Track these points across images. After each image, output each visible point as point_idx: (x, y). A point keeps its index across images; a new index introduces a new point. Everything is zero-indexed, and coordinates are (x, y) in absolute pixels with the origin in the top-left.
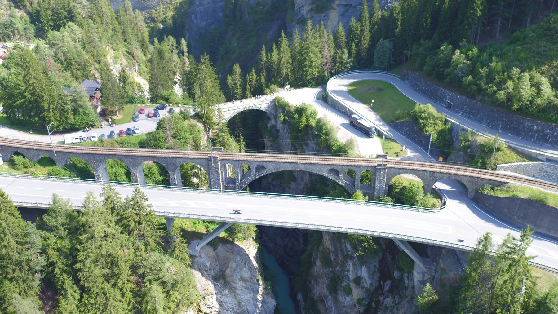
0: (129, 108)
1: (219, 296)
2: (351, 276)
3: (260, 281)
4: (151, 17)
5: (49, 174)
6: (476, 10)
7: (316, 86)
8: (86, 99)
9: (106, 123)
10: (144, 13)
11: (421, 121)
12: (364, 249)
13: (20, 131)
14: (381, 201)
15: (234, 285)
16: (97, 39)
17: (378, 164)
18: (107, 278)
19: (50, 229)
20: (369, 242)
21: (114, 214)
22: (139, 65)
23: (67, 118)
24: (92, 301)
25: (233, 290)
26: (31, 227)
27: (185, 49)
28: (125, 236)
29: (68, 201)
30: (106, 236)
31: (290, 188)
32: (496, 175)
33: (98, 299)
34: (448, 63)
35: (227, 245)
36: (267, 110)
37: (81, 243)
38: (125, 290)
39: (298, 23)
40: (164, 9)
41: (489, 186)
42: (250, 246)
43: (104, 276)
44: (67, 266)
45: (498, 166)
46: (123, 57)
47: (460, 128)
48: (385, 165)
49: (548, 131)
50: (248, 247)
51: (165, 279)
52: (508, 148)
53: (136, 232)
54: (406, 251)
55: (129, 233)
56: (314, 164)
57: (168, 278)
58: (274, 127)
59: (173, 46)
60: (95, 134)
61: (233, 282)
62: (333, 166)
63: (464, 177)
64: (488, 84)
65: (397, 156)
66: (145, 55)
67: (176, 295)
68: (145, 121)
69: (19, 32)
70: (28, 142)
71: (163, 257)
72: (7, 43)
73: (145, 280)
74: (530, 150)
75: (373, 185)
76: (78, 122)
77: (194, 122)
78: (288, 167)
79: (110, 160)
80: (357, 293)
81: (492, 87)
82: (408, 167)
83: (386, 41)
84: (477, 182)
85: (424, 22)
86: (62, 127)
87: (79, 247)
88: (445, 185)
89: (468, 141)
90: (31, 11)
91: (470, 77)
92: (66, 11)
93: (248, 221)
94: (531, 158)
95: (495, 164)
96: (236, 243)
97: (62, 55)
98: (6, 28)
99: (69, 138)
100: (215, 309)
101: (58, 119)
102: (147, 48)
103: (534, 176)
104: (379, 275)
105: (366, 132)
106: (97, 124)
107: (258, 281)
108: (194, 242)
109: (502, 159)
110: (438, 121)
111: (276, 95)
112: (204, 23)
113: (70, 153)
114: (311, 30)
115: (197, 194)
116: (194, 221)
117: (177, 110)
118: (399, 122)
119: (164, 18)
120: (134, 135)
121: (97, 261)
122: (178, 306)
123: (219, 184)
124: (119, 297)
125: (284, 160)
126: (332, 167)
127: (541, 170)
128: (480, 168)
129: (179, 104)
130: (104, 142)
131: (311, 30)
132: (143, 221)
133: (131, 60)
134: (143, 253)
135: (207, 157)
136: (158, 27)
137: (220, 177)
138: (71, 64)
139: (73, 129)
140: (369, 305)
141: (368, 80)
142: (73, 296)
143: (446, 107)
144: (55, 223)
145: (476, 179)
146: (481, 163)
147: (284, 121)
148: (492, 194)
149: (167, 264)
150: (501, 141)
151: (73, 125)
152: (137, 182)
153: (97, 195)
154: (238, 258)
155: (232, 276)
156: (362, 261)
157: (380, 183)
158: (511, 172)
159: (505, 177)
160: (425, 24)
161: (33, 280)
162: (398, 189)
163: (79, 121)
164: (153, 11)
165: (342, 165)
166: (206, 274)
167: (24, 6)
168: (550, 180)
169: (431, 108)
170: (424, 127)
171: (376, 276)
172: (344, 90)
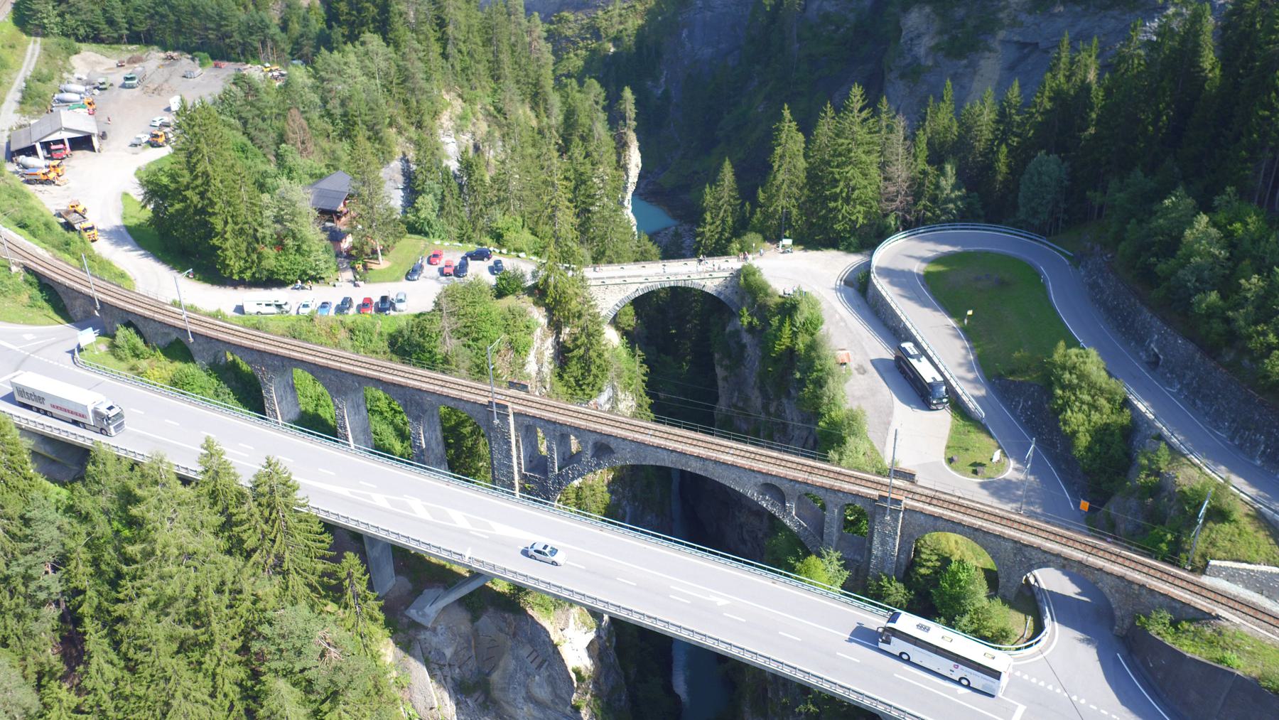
7: (849, 249)
10: (580, 15)
11: (1059, 392)
17: (880, 496)
21: (216, 508)
23: (261, 257)
32: (1197, 589)
34: (1172, 244)
35: (506, 615)
36: (720, 293)
38: (221, 681)
40: (623, 11)
41: (1167, 616)
45: (1212, 562)
46: (480, 116)
47: (1154, 433)
48: (898, 502)
50: (562, 627)
57: (321, 675)
59: (597, 103)
61: (508, 703)
62: (770, 478)
63: (1104, 576)
64: (1256, 323)
65: (975, 472)
66: (537, 116)
70: (152, 302)
75: (867, 545)
76: (282, 266)
78: (664, 460)
81: (1264, 334)
83: (1053, 157)
84: (1138, 596)
85: (1149, 124)
88: (1065, 580)
89: (1158, 473)
91: (1213, 296)
95: (1203, 556)
96: (530, 612)
97: (338, 106)
98: (251, 34)
99: (254, 299)
101: (244, 255)
102: (545, 101)
108: (429, 593)
109: (1228, 545)
110: (1102, 402)
111: (754, 261)
114: (861, 110)
115: (444, 486)
118: (1014, 382)
119: (621, 32)
120: (392, 313)
125: (657, 441)
128: (1164, 560)
129: (522, 251)
131: (861, 110)
136: (605, 50)
139: (271, 281)
141: (987, 253)
143: (1147, 363)
145: (1136, 587)
146: (1169, 543)
148: (1169, 640)
151: (272, 272)
154: (525, 652)
157: (883, 543)
158: (1247, 587)
159: (1219, 598)
160: (1151, 128)
162: (928, 567)
164: (600, 13)
165: (791, 480)
166: (439, 673)
169: (1093, 363)
170: (1063, 409)
172: (915, 271)
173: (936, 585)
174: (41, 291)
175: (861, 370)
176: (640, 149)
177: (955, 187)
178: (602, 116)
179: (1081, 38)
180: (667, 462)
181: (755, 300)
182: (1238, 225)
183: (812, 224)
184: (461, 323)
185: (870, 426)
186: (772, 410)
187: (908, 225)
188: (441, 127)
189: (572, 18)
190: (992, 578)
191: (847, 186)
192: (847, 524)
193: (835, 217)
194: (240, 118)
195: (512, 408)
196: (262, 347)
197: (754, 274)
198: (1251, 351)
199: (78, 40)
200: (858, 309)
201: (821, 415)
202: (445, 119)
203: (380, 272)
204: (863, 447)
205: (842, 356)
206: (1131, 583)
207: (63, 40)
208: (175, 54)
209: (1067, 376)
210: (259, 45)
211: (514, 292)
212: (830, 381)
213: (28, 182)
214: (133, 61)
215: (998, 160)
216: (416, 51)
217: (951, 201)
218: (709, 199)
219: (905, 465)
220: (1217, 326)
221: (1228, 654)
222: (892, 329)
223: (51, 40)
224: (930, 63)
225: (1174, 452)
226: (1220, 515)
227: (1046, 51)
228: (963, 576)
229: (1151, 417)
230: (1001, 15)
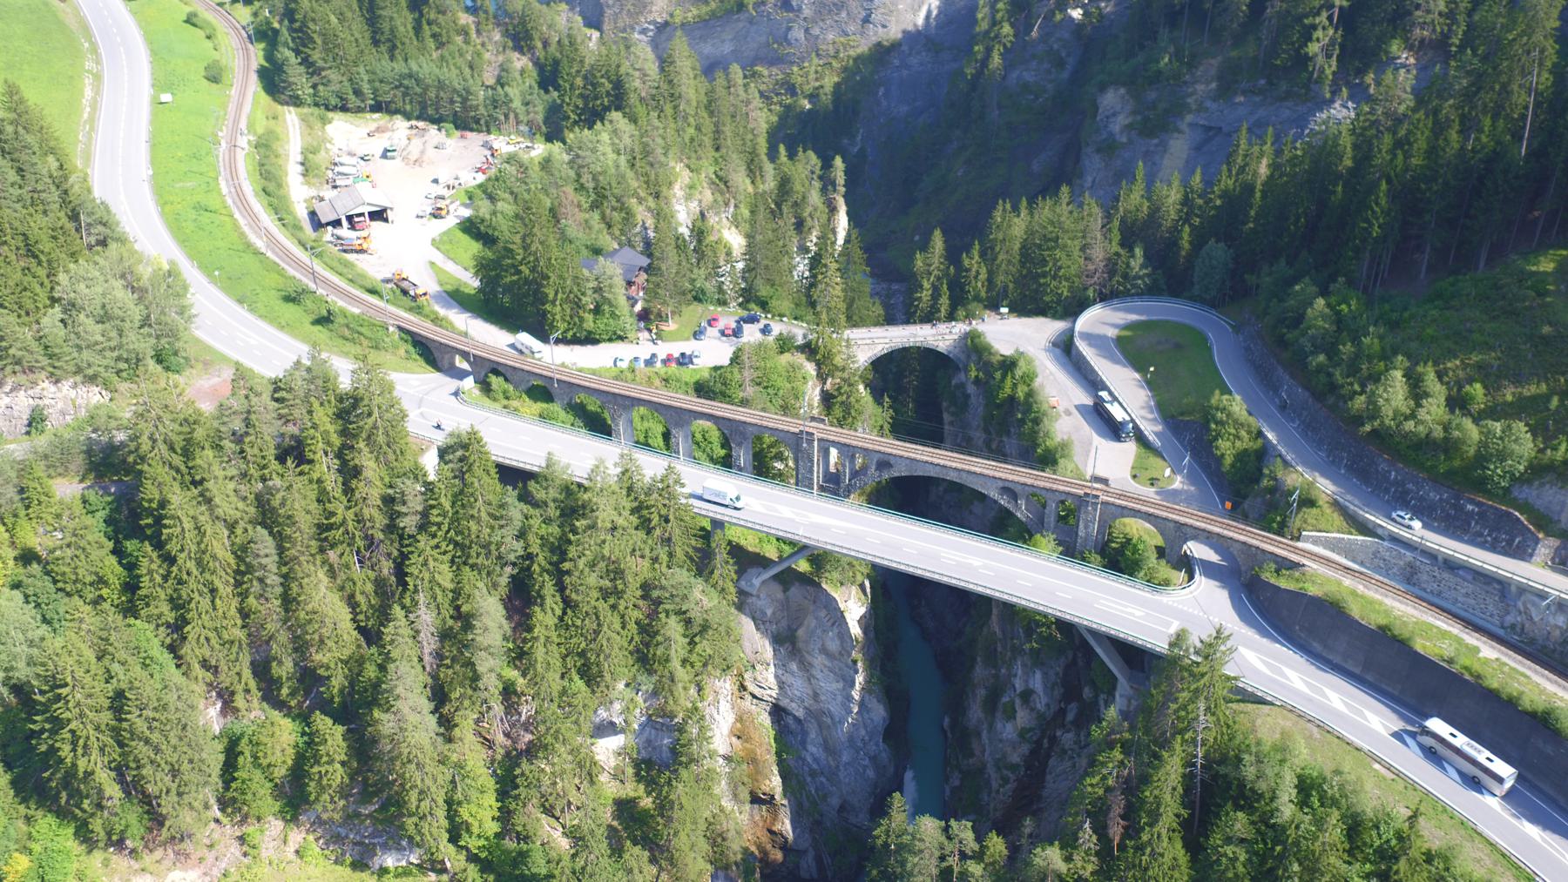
0: (695, 312)
1: (780, 672)
2: (1019, 685)
3: (860, 664)
4: (787, 83)
5: (540, 416)
6: (1371, 224)
7: (1056, 316)
8: (619, 282)
9: (646, 334)
10: (775, 70)
11: (1213, 426)
12: (1043, 639)
13: (501, 328)
14: (1083, 559)
15: (809, 658)
16: (659, 151)
18: (605, 594)
19: (536, 504)
20: (1049, 627)
22: (736, 206)
23: (582, 320)
24: (579, 623)
25: (806, 667)
26: (511, 495)
27: (840, 177)
28: (641, 534)
29: (568, 466)
30: (614, 529)
31: (971, 512)
33: (587, 622)
34: (1298, 319)
37: (575, 532)
39: (1098, 151)
41: (1273, 566)
42: (849, 598)
43: (601, 589)
44: (550, 564)
48: (1097, 497)
49: (1410, 486)
51: (691, 614)
52: (1332, 504)
53: (658, 532)
54: (1099, 650)
55: (649, 532)
56: (975, 473)
57: (695, 614)
58: (962, 386)
59: (813, 172)
60: (622, 353)
66: (753, 182)
67: (704, 647)
68: (717, 342)
69: (516, 116)
71: (692, 580)
72: (493, 136)
73: (660, 610)
74: (1367, 516)
77: (800, 359)
79: (642, 408)
80: (1023, 717)
81: (1351, 384)
82: (1138, 507)
83: (1221, 245)
86: (571, 333)
87: (572, 538)
89: (1275, 479)
90: (543, 60)
91: (1322, 358)
92: (610, 82)
93: (853, 553)
94: (1364, 528)
96: (824, 586)
98: (496, 107)
100: (769, 692)
101: (568, 318)
102: (761, 168)
103: (1362, 564)
104: (1062, 690)
105: (1114, 430)
106: (631, 335)
107: (855, 662)
108: (752, 571)
110: (1243, 433)
111: (976, 325)
112: (904, 109)
113: (579, 386)
116: (761, 535)
117: (777, 328)
119: (817, 88)
121: (594, 565)
122: (705, 665)
123: (812, 479)
124: (617, 626)
125: (925, 458)
126: (1007, 484)
127: (1376, 554)
130: (637, 373)
132: (671, 517)
133: (722, 193)
134: (664, 569)
135: (797, 430)
137: (815, 469)
138: (605, 197)
139: (590, 340)
140: (1039, 743)
141: (1167, 321)
142: (552, 609)
144: (544, 496)
147: (977, 381)
148: (1272, 581)
149: (697, 594)
150: (1325, 487)
151: (590, 332)
152: (678, 453)
153: (610, 464)
155: (807, 642)
156: (1037, 660)
157: (1086, 527)
161: (501, 575)
163: (602, 327)
164: (795, 69)
167: (531, 48)
168: (1387, 576)
169: (1237, 405)
170: (1216, 439)
171: (1056, 692)
173: (1123, 554)
174: (414, 347)
175: (1068, 413)
176: (848, 213)
177: (1143, 266)
178: (817, 184)
179: (1257, 131)
180: (932, 473)
181: (980, 358)
182: (1344, 307)
183: (1025, 296)
184: (755, 375)
185: (1077, 451)
186: (994, 446)
187: (1103, 298)
188: (674, 196)
189: (766, 73)
190: (1161, 552)
191: (1054, 265)
192: (1061, 519)
193: (1045, 290)
194: (512, 193)
195: (817, 435)
196: (616, 391)
197: (979, 337)
198: (1343, 396)
199: (327, 108)
200: (1063, 366)
201: (1039, 445)
202: (678, 191)
203: (670, 332)
204: (1070, 466)
205: (1053, 401)
206: (1251, 546)
207: (316, 111)
208: (421, 124)
209: (1219, 414)
210: (502, 118)
211: (789, 350)
212: (1045, 419)
213: (345, 251)
214: (379, 130)
215: (1182, 238)
216: (657, 128)
217: (1140, 278)
218: (919, 263)
219: (1101, 473)
220: (1322, 378)
221: (1306, 585)
222: (1093, 383)
223: (306, 110)
224: (1124, 140)
225: (1286, 464)
226: (1308, 502)
227: (1229, 135)
228: (1141, 547)
229: (1275, 442)
230: (1189, 100)
